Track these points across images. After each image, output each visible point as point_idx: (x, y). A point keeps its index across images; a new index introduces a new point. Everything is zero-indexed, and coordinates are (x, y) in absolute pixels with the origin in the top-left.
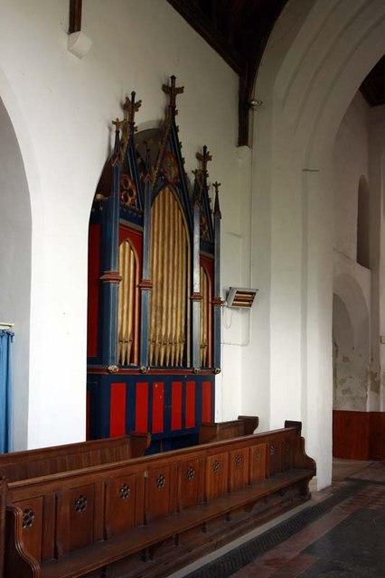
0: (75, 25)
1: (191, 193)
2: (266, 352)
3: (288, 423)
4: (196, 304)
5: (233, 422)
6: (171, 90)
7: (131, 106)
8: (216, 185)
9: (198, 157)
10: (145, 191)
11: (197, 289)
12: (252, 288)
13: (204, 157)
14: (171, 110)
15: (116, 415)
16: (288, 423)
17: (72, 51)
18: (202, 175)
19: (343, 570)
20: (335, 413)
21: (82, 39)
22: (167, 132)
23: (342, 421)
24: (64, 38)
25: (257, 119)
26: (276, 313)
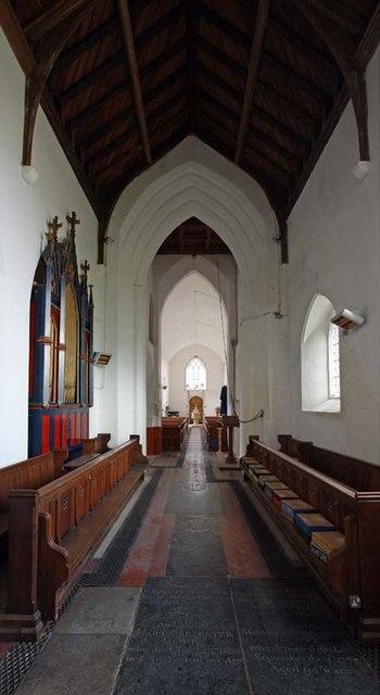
0: (26, 161)
1: (331, 525)
2: (116, 390)
3: (132, 437)
4: (62, 353)
5: (23, 463)
6: (72, 220)
7: (54, 225)
8: (91, 286)
9: (50, 225)
10: (59, 279)
11: (62, 341)
12: (107, 353)
13: (86, 268)
14: (72, 233)
15: (45, 439)
16: (132, 437)
17: (24, 178)
18: (85, 278)
19: (257, 317)
20: (148, 429)
21: (32, 173)
22: (70, 243)
23: (149, 430)
24: (20, 167)
25: (109, 249)
26: (120, 369)
